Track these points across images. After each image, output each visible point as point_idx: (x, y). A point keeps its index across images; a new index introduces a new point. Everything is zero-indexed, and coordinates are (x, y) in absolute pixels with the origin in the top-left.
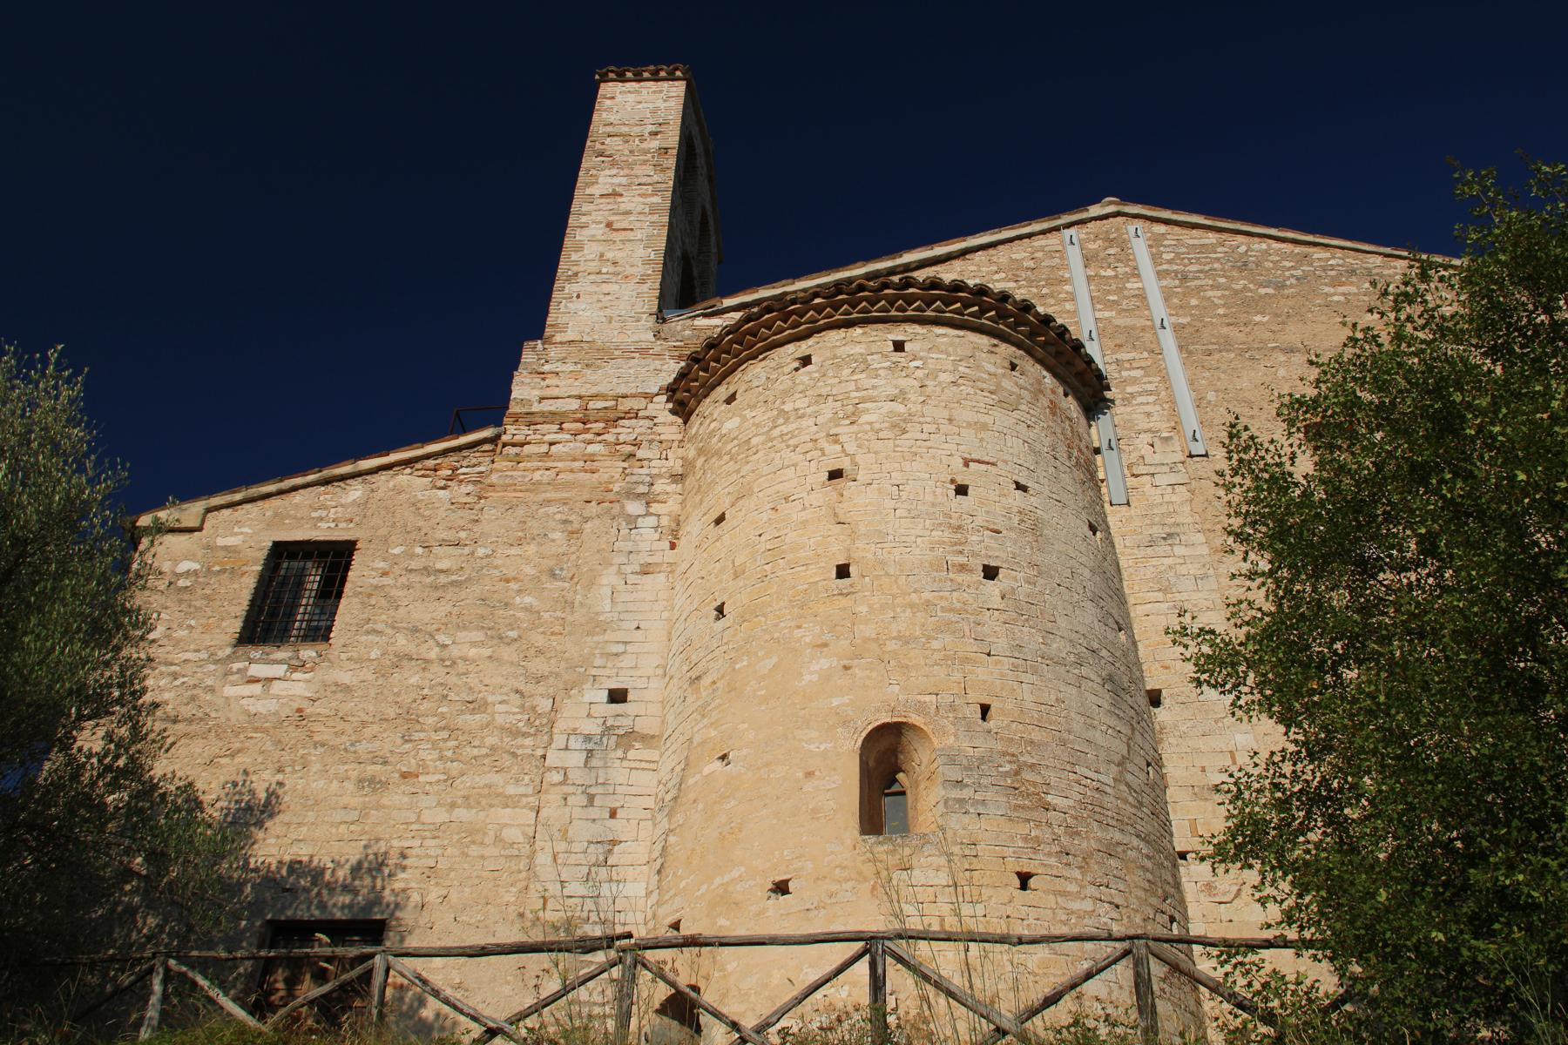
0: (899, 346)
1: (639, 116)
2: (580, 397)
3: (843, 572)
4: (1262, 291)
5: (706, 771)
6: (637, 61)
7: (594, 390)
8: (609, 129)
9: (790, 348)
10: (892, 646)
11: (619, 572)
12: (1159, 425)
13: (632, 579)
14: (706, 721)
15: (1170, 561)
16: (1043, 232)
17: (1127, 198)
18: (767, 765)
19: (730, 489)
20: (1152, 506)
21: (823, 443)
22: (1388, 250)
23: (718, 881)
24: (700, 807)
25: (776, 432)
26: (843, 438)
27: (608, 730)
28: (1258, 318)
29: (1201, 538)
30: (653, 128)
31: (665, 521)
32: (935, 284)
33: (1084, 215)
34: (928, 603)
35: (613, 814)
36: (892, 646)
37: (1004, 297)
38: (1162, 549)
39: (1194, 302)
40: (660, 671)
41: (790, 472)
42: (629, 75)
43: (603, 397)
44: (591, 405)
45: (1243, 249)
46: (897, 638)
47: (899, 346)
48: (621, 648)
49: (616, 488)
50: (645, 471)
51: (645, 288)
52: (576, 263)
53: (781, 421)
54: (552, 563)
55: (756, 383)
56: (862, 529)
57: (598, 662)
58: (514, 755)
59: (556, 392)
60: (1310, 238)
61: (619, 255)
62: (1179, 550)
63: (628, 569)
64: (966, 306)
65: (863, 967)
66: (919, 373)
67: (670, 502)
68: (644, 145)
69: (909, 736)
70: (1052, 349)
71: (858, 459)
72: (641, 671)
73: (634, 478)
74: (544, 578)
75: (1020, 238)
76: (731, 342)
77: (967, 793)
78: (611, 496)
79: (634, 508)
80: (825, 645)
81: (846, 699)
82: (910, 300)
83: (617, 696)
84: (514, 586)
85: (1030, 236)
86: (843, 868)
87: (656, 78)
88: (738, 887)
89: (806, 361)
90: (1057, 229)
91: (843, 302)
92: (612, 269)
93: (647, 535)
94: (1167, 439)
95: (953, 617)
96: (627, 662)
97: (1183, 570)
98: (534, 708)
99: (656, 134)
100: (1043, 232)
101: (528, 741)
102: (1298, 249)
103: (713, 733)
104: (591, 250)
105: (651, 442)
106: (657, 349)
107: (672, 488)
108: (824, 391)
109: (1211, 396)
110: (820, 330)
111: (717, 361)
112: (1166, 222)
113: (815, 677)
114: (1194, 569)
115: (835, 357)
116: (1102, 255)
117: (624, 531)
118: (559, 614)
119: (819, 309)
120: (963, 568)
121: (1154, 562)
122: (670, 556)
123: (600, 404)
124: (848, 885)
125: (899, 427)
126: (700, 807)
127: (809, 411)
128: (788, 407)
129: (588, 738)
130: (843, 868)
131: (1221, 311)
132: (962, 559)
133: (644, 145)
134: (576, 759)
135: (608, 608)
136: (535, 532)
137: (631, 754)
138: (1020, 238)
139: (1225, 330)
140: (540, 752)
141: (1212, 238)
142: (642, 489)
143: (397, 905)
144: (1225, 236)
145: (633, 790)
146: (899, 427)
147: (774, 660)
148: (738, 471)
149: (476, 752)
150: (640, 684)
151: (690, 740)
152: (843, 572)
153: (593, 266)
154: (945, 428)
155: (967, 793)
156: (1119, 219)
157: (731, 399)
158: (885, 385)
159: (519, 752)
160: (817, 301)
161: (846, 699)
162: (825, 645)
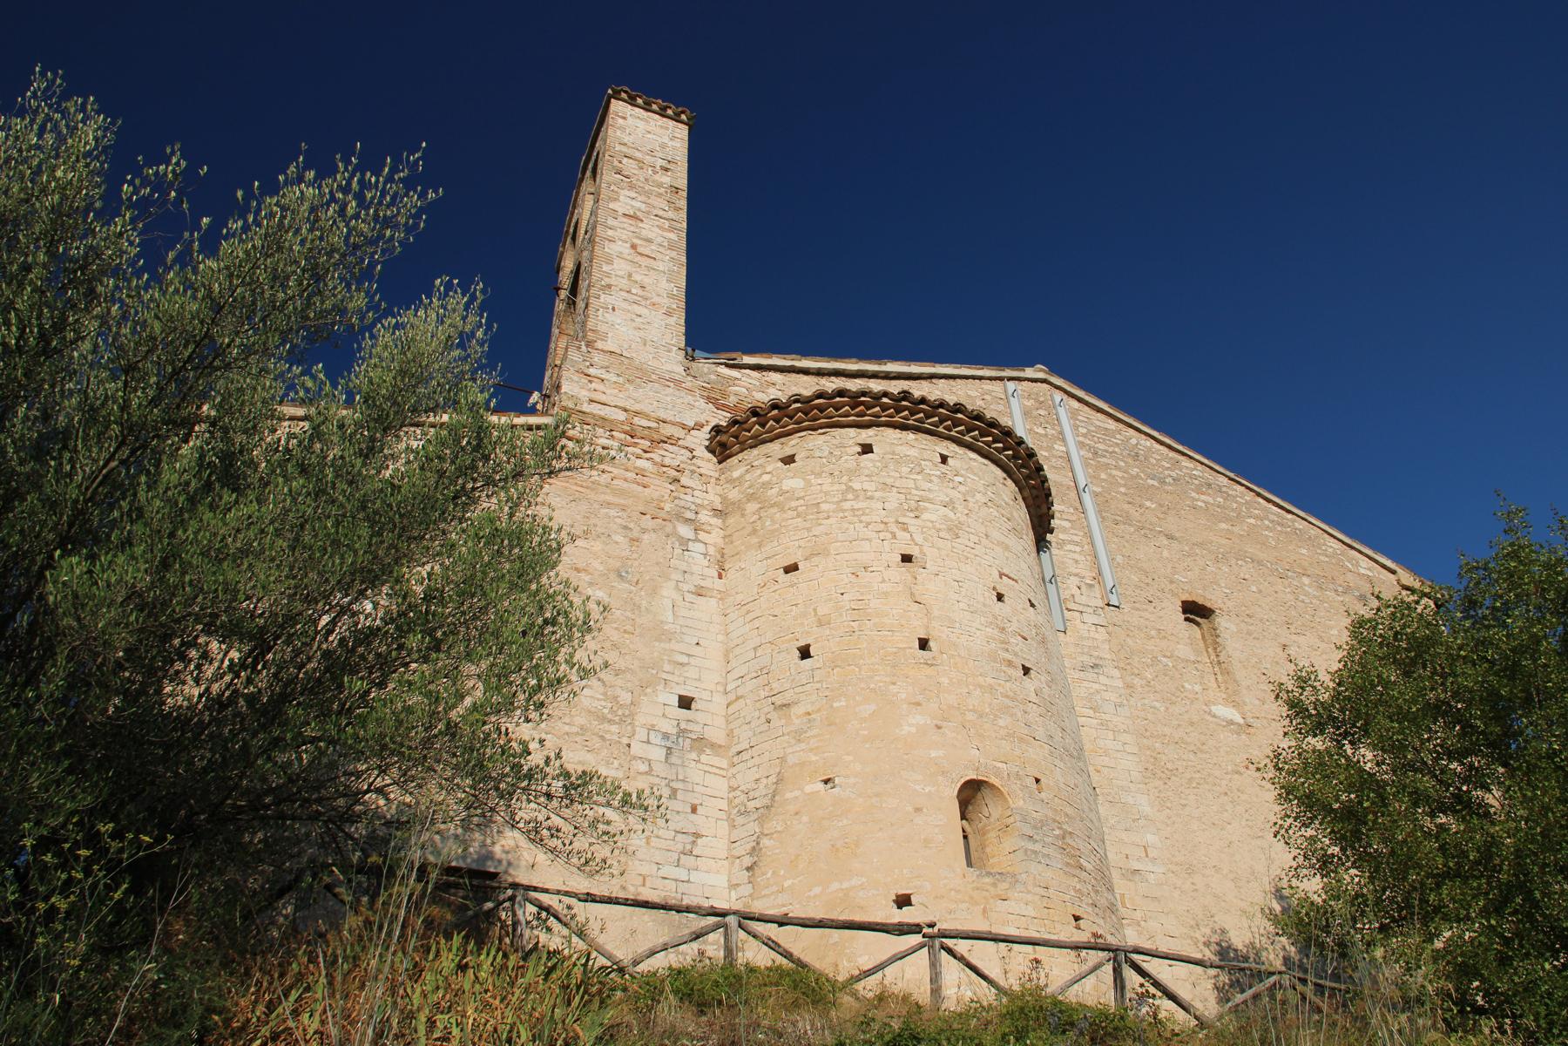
0: (944, 459)
1: (645, 146)
2: (626, 410)
3: (924, 644)
4: (1150, 482)
5: (808, 789)
6: (655, 91)
7: (637, 407)
8: (624, 149)
9: (852, 432)
10: (970, 716)
11: (677, 588)
12: (1084, 573)
13: (689, 597)
14: (803, 746)
15: (1096, 686)
16: (990, 379)
17: (1053, 370)
18: (877, 795)
19: (802, 543)
20: (1082, 638)
21: (893, 528)
22: (1232, 475)
23: (835, 886)
24: (805, 819)
25: (847, 505)
26: (911, 529)
27: (682, 732)
28: (1148, 504)
29: (1116, 673)
30: (664, 163)
31: (711, 550)
32: (906, 395)
33: (1021, 374)
34: (991, 687)
35: (694, 810)
36: (970, 716)
37: (1021, 442)
38: (1090, 675)
39: (1103, 476)
40: (721, 688)
41: (866, 546)
42: (640, 101)
43: (648, 417)
44: (636, 420)
45: (1134, 441)
46: (974, 711)
47: (944, 459)
48: (684, 659)
49: (667, 507)
50: (689, 498)
51: (672, 321)
52: (608, 275)
53: (850, 496)
54: (618, 564)
55: (818, 454)
56: (936, 613)
57: (667, 667)
58: (602, 737)
59: (603, 398)
60: (1180, 448)
61: (647, 281)
62: (1103, 679)
63: (685, 587)
64: (995, 441)
65: (1109, 968)
66: (962, 488)
67: (714, 534)
68: (657, 177)
69: (985, 791)
70: (1035, 492)
71: (925, 549)
72: (704, 682)
73: (682, 503)
74: (613, 576)
75: (974, 377)
76: (798, 410)
77: (1037, 847)
78: (662, 514)
79: (685, 531)
80: (919, 704)
81: (941, 753)
82: (956, 423)
83: (685, 703)
84: (585, 577)
85: (981, 378)
86: (958, 891)
87: (662, 113)
88: (861, 894)
89: (867, 449)
90: (1001, 379)
91: (906, 408)
92: (640, 292)
93: (699, 562)
94: (1091, 586)
95: (1007, 701)
96: (692, 673)
97: (1106, 695)
98: (615, 698)
99: (667, 170)
100: (990, 379)
101: (614, 728)
102: (1172, 454)
103: (814, 758)
104: (620, 267)
105: (693, 472)
106: (688, 385)
107: (714, 521)
108: (889, 481)
109: (1119, 559)
110: (879, 425)
111: (777, 421)
112: (1080, 400)
113: (913, 730)
114: (1113, 697)
115: (893, 453)
116: (1035, 413)
117: (678, 551)
118: (629, 614)
119: (884, 408)
120: (1010, 664)
121: (1085, 684)
122: (718, 584)
123: (645, 423)
124: (964, 906)
125: (955, 530)
126: (805, 819)
127: (877, 494)
128: (856, 486)
129: (666, 736)
130: (958, 891)
131: (1123, 490)
132: (1008, 656)
133: (657, 177)
134: (658, 754)
135: (670, 619)
136: (600, 530)
137: (704, 758)
138: (974, 377)
139: (1126, 506)
140: (625, 741)
141: (1112, 425)
142: (689, 515)
143: (509, 864)
144: (1121, 426)
145: (709, 792)
146: (955, 530)
147: (873, 707)
148: (809, 530)
149: (567, 728)
150: (706, 695)
151: (783, 759)
152: (924, 644)
153: (624, 283)
154: (984, 541)
155: (1037, 847)
156: (1045, 386)
157: (789, 460)
158: (940, 492)
159: (608, 736)
160: (885, 400)
161: (941, 753)
162: (919, 704)
